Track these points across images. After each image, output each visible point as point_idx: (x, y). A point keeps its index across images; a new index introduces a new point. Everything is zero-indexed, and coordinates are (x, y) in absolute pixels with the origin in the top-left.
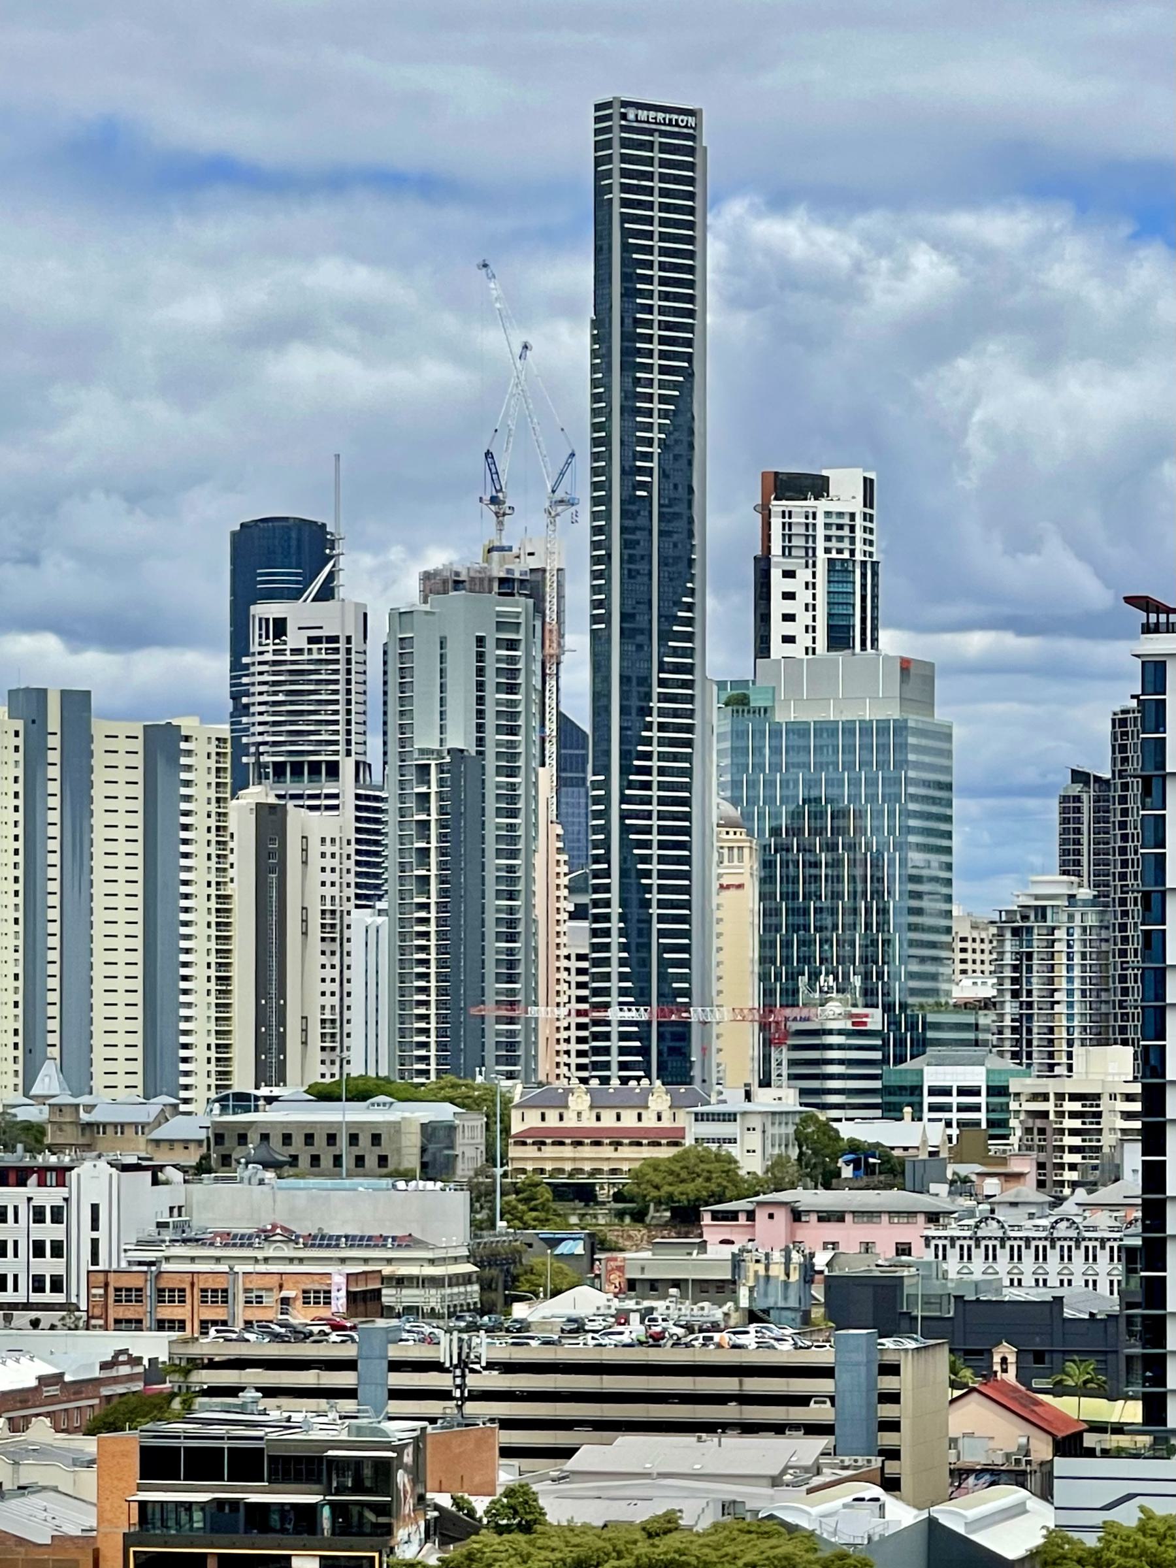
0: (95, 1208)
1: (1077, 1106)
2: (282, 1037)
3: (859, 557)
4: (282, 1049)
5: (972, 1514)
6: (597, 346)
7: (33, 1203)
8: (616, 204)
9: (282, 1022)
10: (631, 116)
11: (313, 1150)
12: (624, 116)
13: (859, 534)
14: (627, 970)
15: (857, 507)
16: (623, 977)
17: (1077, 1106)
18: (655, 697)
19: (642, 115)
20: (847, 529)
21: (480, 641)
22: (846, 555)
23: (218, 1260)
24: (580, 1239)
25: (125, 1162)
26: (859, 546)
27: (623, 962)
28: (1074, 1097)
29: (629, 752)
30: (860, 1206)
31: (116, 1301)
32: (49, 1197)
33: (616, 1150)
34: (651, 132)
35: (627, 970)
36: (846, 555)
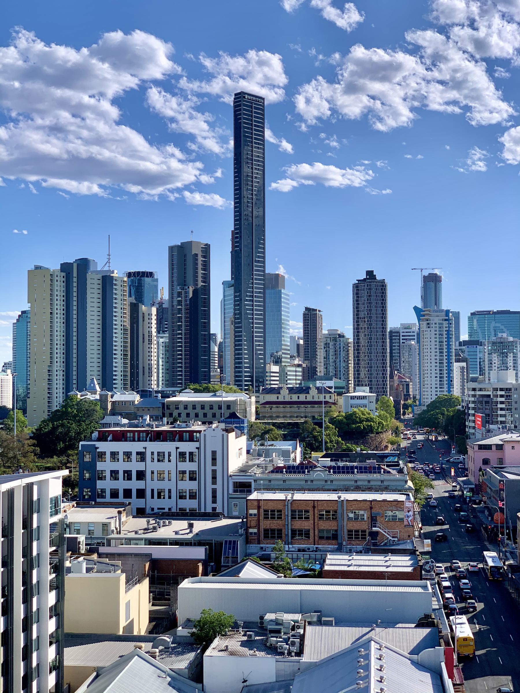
0: (214, 453)
1: (503, 393)
2: (138, 373)
4: (138, 377)
5: (488, 555)
7: (179, 450)
9: (138, 368)
10: (246, 97)
11: (196, 411)
12: (244, 97)
17: (503, 393)
19: (249, 97)
24: (396, 456)
28: (501, 390)
31: (265, 518)
32: (187, 447)
33: (299, 409)
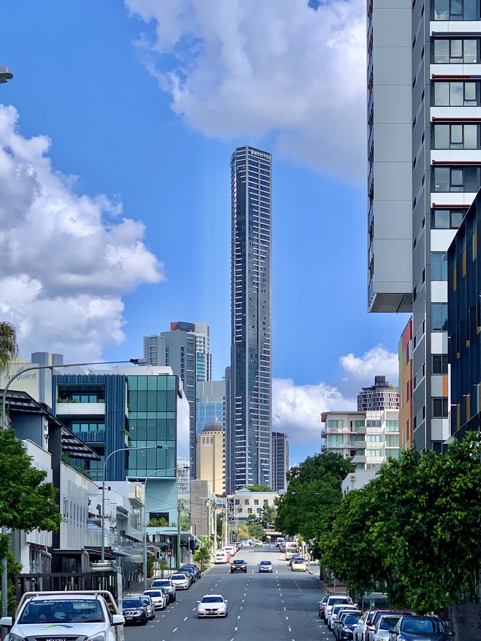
3: (206, 353)
8: (247, 184)
10: (252, 153)
12: (250, 152)
15: (205, 335)
18: (259, 368)
19: (256, 153)
20: (202, 343)
21: (182, 348)
22: (202, 352)
23: (92, 594)
34: (257, 160)
36: (202, 352)
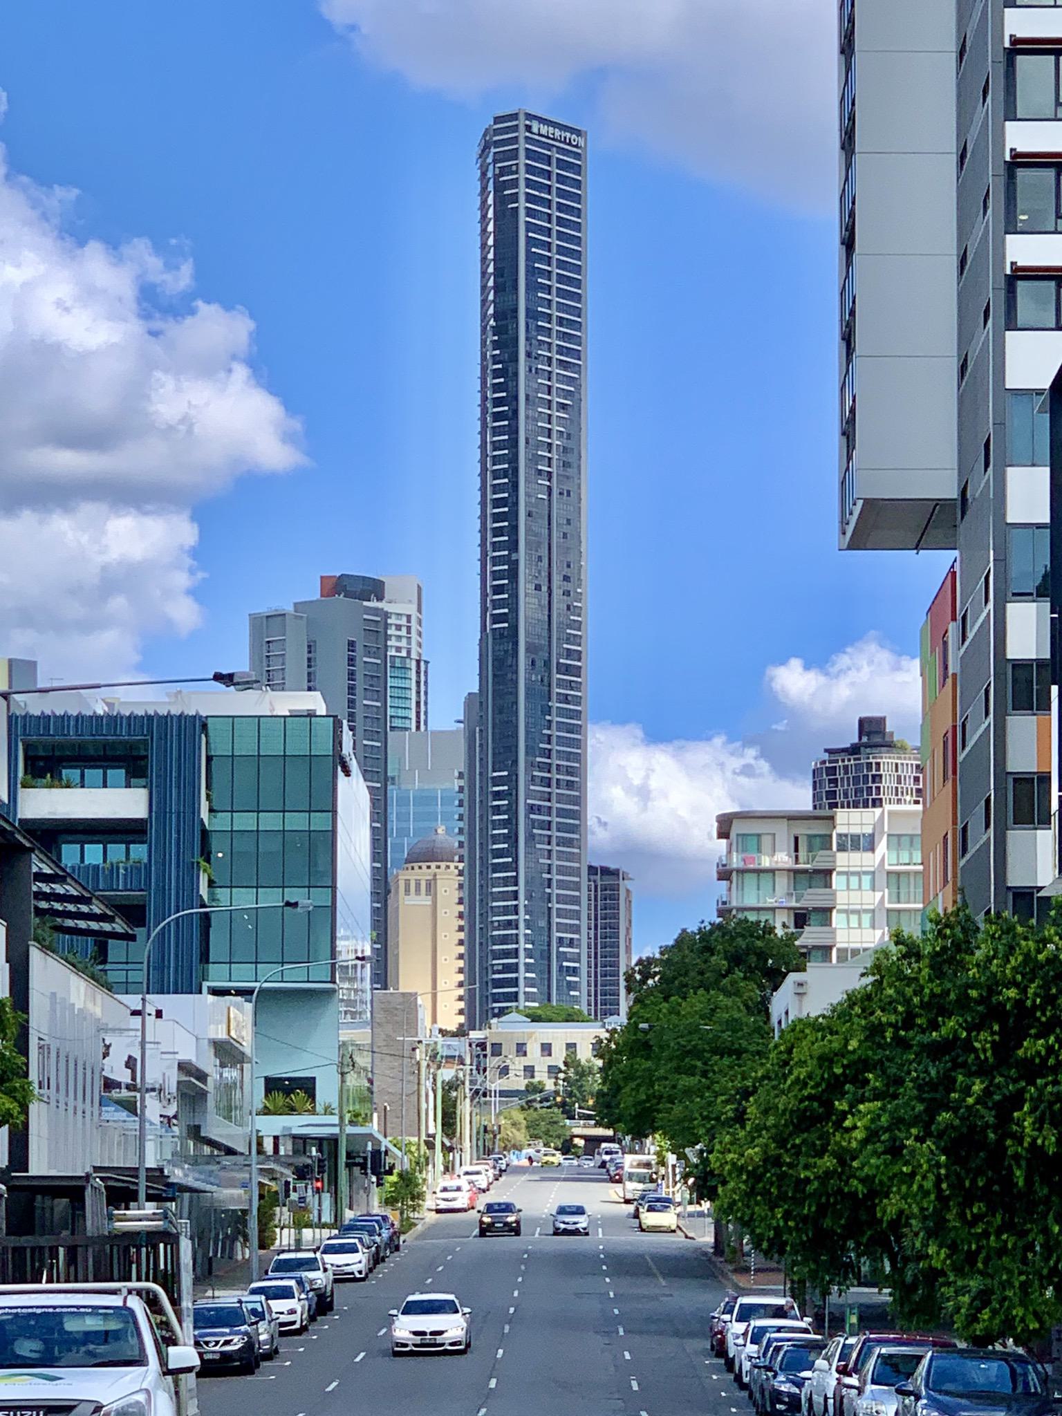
3: (414, 655)
6: (497, 352)
8: (522, 213)
10: (535, 130)
12: (528, 128)
13: (414, 635)
14: (532, 961)
15: (412, 609)
16: (529, 968)
18: (554, 697)
20: (404, 630)
21: (351, 644)
22: (404, 654)
25: (31, 1106)
26: (414, 646)
27: (529, 954)
29: (533, 748)
30: (89, 1373)
35: (532, 961)
36: (404, 654)
